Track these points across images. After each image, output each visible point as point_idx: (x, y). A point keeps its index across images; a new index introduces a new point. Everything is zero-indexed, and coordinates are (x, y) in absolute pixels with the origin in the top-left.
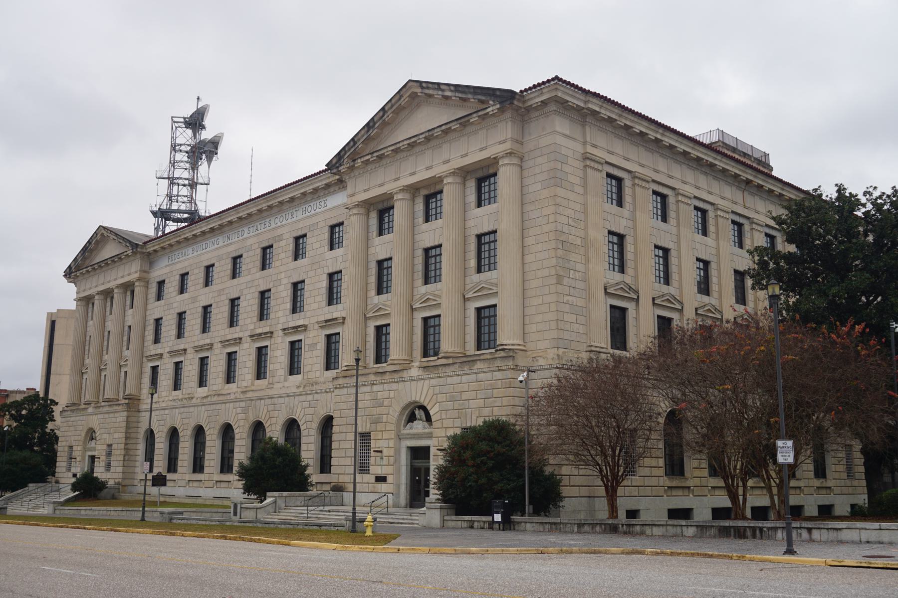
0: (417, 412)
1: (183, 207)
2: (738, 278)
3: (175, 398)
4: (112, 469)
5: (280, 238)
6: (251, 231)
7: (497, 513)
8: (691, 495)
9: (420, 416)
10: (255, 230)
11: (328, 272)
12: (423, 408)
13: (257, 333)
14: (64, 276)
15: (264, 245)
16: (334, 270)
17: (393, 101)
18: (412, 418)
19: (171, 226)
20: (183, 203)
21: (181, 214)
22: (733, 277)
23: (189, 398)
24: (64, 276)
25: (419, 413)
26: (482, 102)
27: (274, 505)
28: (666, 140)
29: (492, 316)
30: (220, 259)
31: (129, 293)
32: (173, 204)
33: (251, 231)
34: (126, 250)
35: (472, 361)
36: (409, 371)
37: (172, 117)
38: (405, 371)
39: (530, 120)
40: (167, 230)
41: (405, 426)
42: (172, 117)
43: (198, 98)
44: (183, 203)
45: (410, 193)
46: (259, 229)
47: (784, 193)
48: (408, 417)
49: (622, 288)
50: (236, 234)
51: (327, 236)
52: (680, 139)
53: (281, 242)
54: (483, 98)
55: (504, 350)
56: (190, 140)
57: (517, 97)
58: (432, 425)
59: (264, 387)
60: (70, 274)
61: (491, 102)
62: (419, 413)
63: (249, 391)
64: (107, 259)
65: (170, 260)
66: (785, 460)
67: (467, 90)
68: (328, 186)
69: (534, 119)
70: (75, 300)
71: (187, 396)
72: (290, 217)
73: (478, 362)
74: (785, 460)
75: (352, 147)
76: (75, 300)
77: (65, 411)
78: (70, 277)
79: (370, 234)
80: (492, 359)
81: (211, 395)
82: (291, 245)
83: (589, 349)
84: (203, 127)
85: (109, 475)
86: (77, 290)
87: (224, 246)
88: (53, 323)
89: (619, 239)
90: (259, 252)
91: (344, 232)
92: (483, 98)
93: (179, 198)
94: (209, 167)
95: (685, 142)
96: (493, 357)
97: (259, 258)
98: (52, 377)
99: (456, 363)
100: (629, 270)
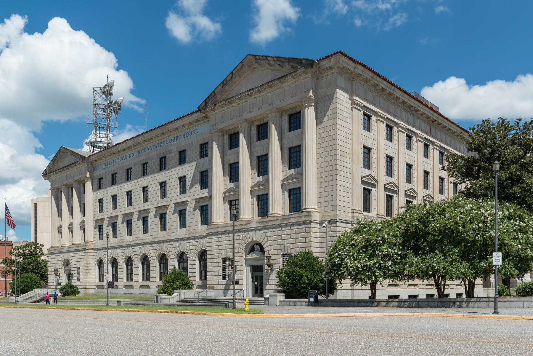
0: (255, 247)
1: (103, 140)
2: (425, 175)
3: (114, 242)
4: (81, 281)
5: (170, 152)
6: (153, 148)
7: (311, 297)
8: (399, 289)
9: (257, 249)
10: (155, 148)
11: (200, 171)
12: (260, 244)
13: (160, 206)
14: (42, 176)
15: (161, 156)
16: (204, 170)
17: (238, 68)
18: (252, 250)
19: (97, 150)
20: (103, 138)
21: (103, 144)
22: (423, 174)
23: (122, 242)
24: (42, 176)
25: (257, 247)
26: (293, 67)
27: (179, 296)
28: (395, 94)
29: (298, 194)
30: (135, 164)
31: (82, 185)
32: (97, 138)
33: (153, 148)
34: (78, 160)
35: (288, 218)
36: (251, 224)
37: (93, 87)
38: (248, 225)
39: (322, 79)
40: (95, 152)
41: (249, 254)
42: (93, 87)
43: (107, 76)
44: (103, 138)
45: (248, 124)
46: (157, 147)
47: (451, 128)
48: (250, 249)
49: (369, 178)
50: (144, 150)
51: (198, 150)
52: (403, 93)
53: (171, 154)
54: (294, 65)
55: (306, 211)
56: (104, 101)
57: (315, 64)
58: (265, 253)
59: (165, 235)
60: (46, 175)
61: (299, 67)
62: (257, 247)
63: (156, 237)
64: (67, 166)
65: (105, 166)
66: (497, 263)
67: (284, 60)
68: (198, 120)
69: (324, 78)
70: (50, 189)
71: (120, 241)
72: (176, 140)
73: (292, 219)
74: (497, 263)
75: (213, 97)
76: (50, 189)
77: (51, 250)
78: (46, 177)
79: (225, 148)
80: (300, 217)
81: (134, 240)
82: (177, 156)
83: (353, 211)
84: (111, 94)
85: (79, 283)
86: (51, 183)
87: (137, 157)
88: (36, 204)
89: (367, 150)
90: (158, 160)
91: (209, 147)
92: (294, 65)
93: (100, 135)
94: (6, 204)
95: (405, 95)
96: (300, 215)
97: (158, 163)
98: (38, 234)
99: (278, 219)
100: (373, 168)
